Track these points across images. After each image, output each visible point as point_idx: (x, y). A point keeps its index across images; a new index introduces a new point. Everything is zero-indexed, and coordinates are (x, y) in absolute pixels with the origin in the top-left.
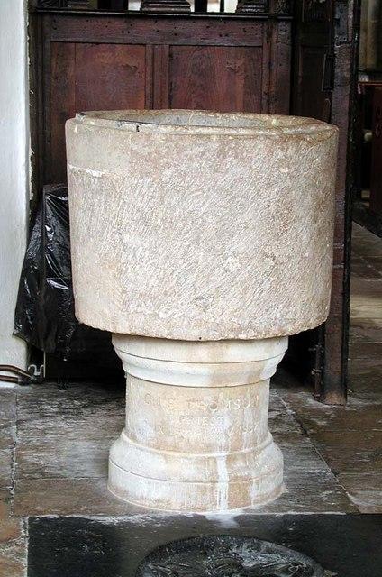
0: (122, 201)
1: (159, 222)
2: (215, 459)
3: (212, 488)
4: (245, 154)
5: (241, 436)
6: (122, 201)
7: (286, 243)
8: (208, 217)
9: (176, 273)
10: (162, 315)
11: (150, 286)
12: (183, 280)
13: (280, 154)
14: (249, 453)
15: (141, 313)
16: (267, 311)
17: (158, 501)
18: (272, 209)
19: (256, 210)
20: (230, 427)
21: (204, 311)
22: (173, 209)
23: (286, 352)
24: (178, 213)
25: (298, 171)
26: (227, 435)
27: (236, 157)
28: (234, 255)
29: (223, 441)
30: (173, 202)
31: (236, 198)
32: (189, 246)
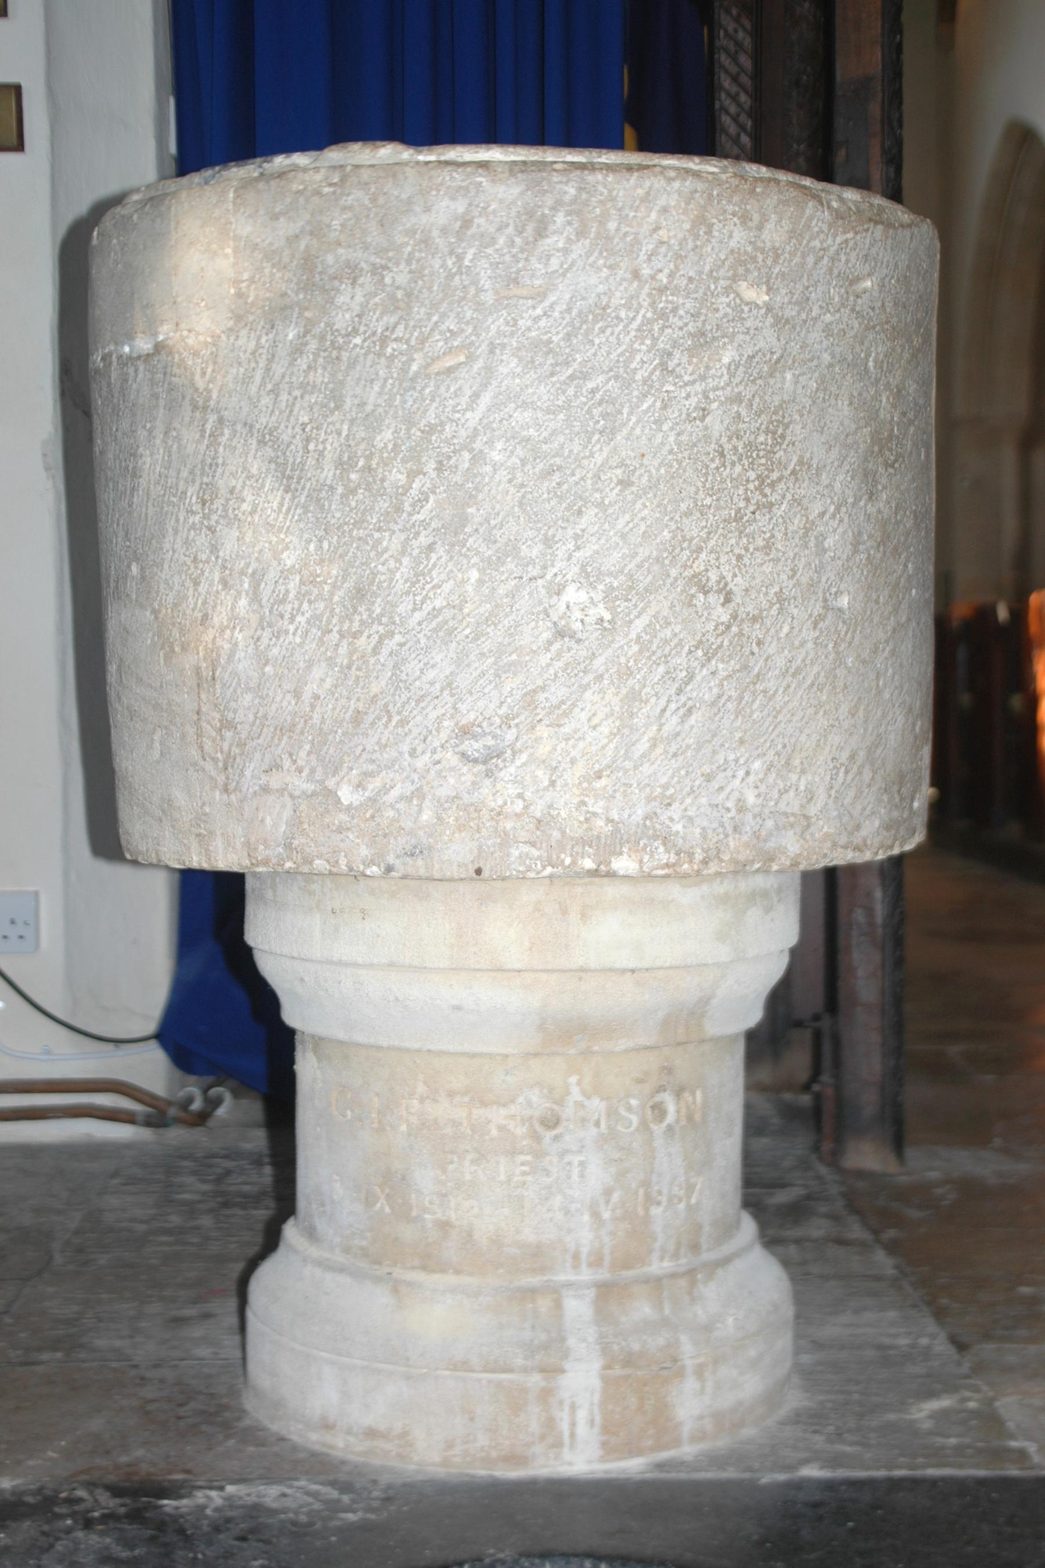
0: (212, 418)
1: (328, 473)
2: (555, 1292)
3: (546, 1395)
4: (612, 225)
5: (647, 1219)
6: (212, 418)
7: (768, 547)
8: (490, 443)
9: (391, 644)
10: (346, 795)
11: (307, 696)
12: (413, 667)
13: (739, 237)
14: (673, 1276)
15: (282, 791)
16: (709, 778)
17: (371, 1433)
18: (717, 423)
19: (658, 422)
20: (608, 1192)
21: (489, 774)
22: (372, 422)
23: (794, 952)
24: (388, 435)
25: (803, 302)
26: (596, 1215)
27: (581, 233)
28: (588, 576)
29: (585, 1237)
30: (372, 397)
31: (585, 377)
32: (431, 548)
